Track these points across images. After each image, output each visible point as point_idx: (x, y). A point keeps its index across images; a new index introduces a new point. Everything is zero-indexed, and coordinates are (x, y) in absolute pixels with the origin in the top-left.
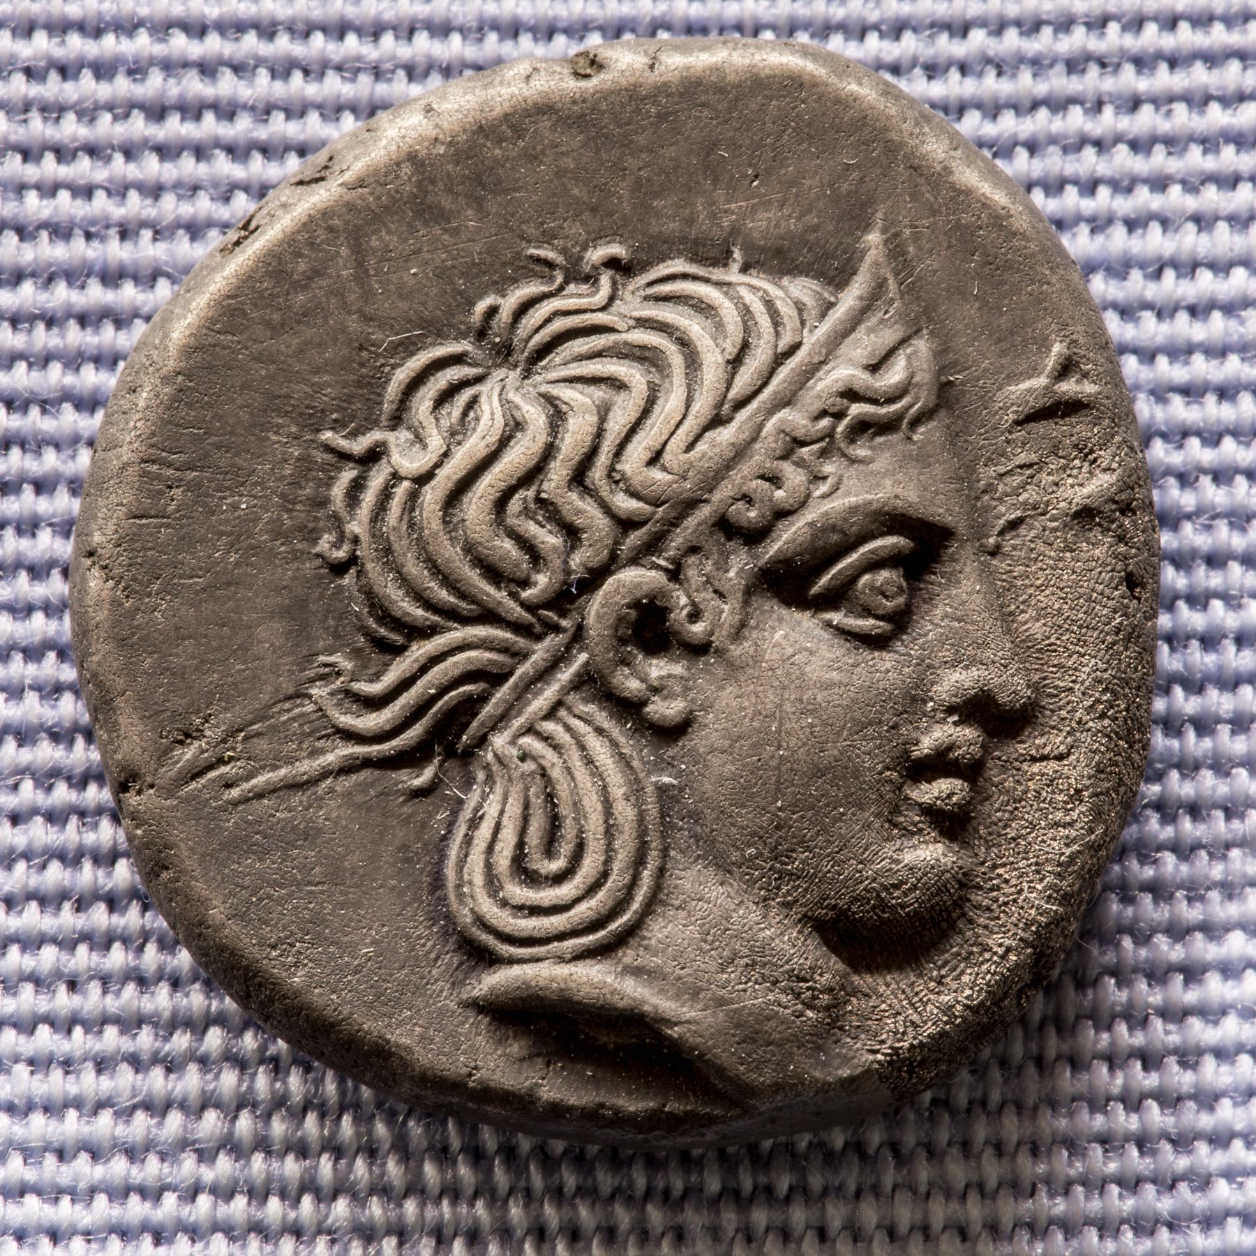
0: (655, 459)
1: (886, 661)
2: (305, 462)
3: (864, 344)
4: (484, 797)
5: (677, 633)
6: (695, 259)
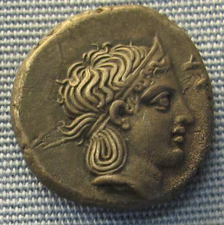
0: (120, 79)
1: (166, 115)
2: (53, 86)
3: (156, 58)
4: (92, 145)
5: (126, 112)
6: (122, 44)
